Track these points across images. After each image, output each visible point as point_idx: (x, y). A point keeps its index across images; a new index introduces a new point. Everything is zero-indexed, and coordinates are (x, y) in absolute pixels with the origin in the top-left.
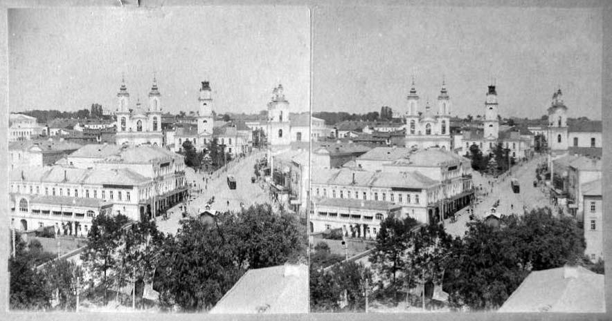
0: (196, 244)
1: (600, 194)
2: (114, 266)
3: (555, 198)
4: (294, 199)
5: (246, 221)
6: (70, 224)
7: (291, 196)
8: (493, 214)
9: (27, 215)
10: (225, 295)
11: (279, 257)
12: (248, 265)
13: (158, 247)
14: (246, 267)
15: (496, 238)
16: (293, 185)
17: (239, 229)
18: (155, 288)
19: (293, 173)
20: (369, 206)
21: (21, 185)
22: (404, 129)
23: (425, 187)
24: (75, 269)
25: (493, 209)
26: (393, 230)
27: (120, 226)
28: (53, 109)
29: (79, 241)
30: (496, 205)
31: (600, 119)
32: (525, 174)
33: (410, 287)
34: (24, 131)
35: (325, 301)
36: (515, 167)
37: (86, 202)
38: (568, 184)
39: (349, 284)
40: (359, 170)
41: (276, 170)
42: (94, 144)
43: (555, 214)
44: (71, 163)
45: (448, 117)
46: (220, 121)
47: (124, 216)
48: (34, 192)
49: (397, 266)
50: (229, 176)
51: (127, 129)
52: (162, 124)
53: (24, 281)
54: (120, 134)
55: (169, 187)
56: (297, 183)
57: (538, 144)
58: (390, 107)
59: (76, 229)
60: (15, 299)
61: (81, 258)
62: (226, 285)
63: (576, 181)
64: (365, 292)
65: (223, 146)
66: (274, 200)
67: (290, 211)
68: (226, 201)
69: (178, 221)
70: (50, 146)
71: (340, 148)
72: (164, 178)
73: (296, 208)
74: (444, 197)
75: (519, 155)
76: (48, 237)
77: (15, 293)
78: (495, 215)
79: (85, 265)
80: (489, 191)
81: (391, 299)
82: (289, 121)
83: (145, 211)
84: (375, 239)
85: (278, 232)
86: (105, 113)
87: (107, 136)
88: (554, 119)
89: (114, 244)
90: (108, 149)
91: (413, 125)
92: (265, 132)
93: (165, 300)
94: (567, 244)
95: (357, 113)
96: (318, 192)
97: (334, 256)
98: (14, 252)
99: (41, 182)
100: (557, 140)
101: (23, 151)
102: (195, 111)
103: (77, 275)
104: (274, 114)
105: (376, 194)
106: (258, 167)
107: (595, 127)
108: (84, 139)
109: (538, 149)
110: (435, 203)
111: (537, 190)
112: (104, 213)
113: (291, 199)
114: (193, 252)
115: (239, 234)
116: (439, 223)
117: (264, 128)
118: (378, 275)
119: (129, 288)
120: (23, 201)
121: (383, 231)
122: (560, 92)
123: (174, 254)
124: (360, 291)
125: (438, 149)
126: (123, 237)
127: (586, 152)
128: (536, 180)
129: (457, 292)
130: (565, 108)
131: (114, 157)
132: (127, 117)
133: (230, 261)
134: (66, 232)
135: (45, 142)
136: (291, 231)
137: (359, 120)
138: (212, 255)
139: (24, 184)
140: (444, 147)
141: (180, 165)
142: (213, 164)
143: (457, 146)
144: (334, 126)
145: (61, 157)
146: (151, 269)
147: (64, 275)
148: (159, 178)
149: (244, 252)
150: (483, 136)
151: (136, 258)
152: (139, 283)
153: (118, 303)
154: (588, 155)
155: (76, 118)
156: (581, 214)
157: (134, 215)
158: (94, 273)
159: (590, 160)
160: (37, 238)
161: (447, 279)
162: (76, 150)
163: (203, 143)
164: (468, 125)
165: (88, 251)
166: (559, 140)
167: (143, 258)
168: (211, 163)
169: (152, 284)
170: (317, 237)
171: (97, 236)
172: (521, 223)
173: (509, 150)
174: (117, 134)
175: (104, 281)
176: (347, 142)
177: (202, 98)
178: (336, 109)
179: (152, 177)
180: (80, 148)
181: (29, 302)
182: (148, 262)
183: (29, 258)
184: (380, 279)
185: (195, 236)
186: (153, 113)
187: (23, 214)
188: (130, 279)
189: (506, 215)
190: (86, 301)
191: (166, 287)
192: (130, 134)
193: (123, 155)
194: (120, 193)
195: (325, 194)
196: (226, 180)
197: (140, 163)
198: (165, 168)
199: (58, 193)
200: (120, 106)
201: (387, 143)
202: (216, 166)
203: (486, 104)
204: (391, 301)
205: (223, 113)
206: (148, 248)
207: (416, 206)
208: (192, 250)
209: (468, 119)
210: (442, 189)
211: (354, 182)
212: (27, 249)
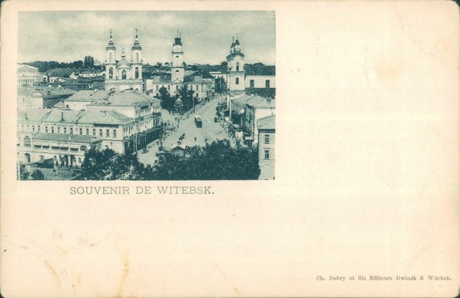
6: (66, 156)
8: (180, 146)
16: (247, 123)
22: (104, 75)
23: (122, 123)
25: (179, 142)
32: (206, 112)
36: (197, 106)
38: (245, 120)
43: (233, 145)
46: (189, 71)
51: (114, 78)
52: (143, 73)
54: (108, 81)
56: (250, 122)
58: (92, 56)
63: (252, 117)
72: (144, 118)
74: (138, 132)
75: (202, 95)
80: (175, 126)
88: (232, 64)
96: (34, 129)
100: (235, 82)
105: (81, 129)
117: (225, 76)
121: (87, 160)
125: (132, 91)
130: (242, 55)
135: (45, 89)
143: (148, 89)
144: (46, 73)
156: (256, 146)
160: (39, 168)
166: (237, 83)
172: (203, 154)
173: (193, 92)
176: (57, 86)
178: (48, 58)
187: (27, 149)
189: (190, 146)
193: (110, 98)
195: (39, 129)
196: (194, 120)
198: (144, 110)
201: (90, 87)
203: (173, 53)
211: (62, 119)
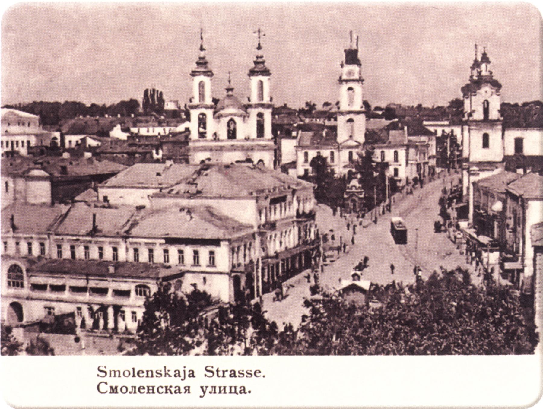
3: (475, 249)
6: (104, 308)
16: (508, 234)
22: (187, 130)
23: (228, 237)
28: (71, 99)
30: (361, 267)
32: (419, 213)
36: (397, 195)
38: (503, 227)
40: (104, 207)
45: (268, 106)
46: (377, 120)
47: (205, 293)
51: (209, 136)
59: (115, 315)
65: (385, 165)
71: (69, 168)
72: (278, 224)
74: (263, 254)
75: (405, 173)
78: (357, 283)
82: (502, 118)
83: (243, 283)
84: (135, 332)
88: (474, 106)
91: (202, 122)
102: (333, 103)
111: (442, 236)
116: (253, 302)
122: (485, 59)
128: (440, 219)
130: (496, 85)
137: (102, 115)
140: (261, 161)
143: (286, 159)
144: (57, 127)
145: (86, 188)
164: (307, 120)
170: (29, 331)
189: (380, 284)
201: (155, 156)
205: (383, 105)
210: (258, 239)
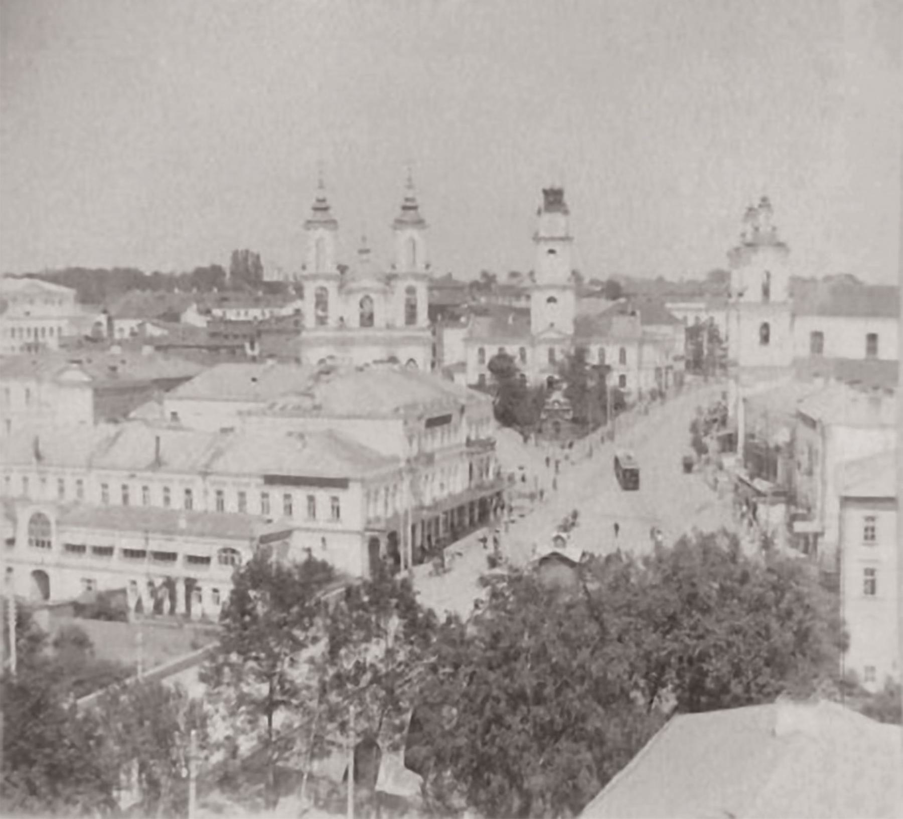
0: (526, 641)
1: (891, 493)
2: (295, 702)
3: (749, 504)
4: (804, 518)
5: (667, 580)
7: (793, 509)
8: (559, 550)
9: (48, 558)
10: (608, 786)
11: (761, 680)
12: (673, 702)
13: (417, 650)
14: (666, 707)
15: (569, 617)
16: (799, 478)
17: (649, 599)
18: (410, 765)
19: (801, 446)
20: (204, 524)
21: (33, 477)
22: (298, 312)
23: (359, 476)
24: (184, 709)
26: (268, 596)
27: (312, 592)
29: (196, 632)
31: (894, 282)
33: (313, 756)
34: (39, 324)
35: (81, 789)
36: (623, 417)
37: (216, 523)
39: (144, 743)
41: (752, 436)
42: (238, 361)
44: (174, 414)
48: (71, 494)
49: (278, 697)
50: (620, 453)
51: (332, 322)
53: (40, 736)
55: (450, 484)
56: (810, 473)
57: (698, 353)
59: (188, 598)
60: (15, 785)
61: (203, 678)
62: (610, 757)
64: (187, 766)
66: (746, 521)
67: (793, 553)
68: (611, 524)
69: (475, 578)
70: (114, 369)
71: (120, 370)
72: (437, 457)
73: (807, 544)
74: (414, 503)
76: (110, 618)
77: (15, 767)
79: (212, 698)
81: (262, 786)
82: (791, 301)
83: (383, 548)
85: (757, 610)
86: (270, 276)
87: (272, 340)
89: (294, 639)
90: (278, 377)
92: (722, 331)
93: (439, 797)
94: (789, 636)
95: (166, 269)
97: (105, 664)
98: (13, 661)
99: (90, 467)
101: (39, 380)
102: (525, 271)
103: (191, 724)
104: (747, 278)
106: (701, 428)
107: (874, 301)
108: (210, 348)
109: (696, 363)
110: (388, 521)
112: (266, 554)
113: (794, 518)
114: (518, 665)
115: (647, 614)
117: (719, 318)
118: (224, 718)
119: (337, 764)
120: (38, 519)
123: (464, 670)
124: (174, 763)
125: (396, 367)
126: (319, 621)
127: (853, 374)
128: (692, 453)
129: (449, 773)
131: (295, 400)
132: (332, 287)
133: (622, 690)
134: (158, 607)
135: (99, 357)
136: (795, 607)
137: (170, 290)
138: (572, 673)
139: (40, 472)
141: (481, 422)
142: (574, 420)
144: (101, 307)
145: (147, 399)
146: (400, 711)
147: (155, 723)
148: (423, 459)
149: (662, 667)
150: (528, 331)
151: (356, 680)
152: (366, 751)
153: (306, 803)
154: (857, 382)
155: (187, 290)
157: (351, 561)
158: (240, 721)
159: (863, 396)
161: (417, 735)
162: (188, 379)
163: (544, 359)
165: (221, 659)
167: (376, 679)
168: (569, 416)
169: (402, 753)
171: (247, 618)
174: (304, 334)
175: (266, 743)
177: (542, 234)
178: (98, 258)
179: (403, 456)
180: (197, 374)
181: (55, 793)
182: (390, 691)
183: (55, 677)
184: (230, 732)
185: (524, 621)
186: (405, 276)
187: (39, 557)
188: (340, 739)
190: (216, 796)
191: (440, 760)
192: (339, 334)
193: (321, 391)
194: (311, 499)
196: (611, 464)
197: (370, 416)
198: (438, 429)
199: (136, 499)
200: (311, 257)
202: (582, 425)
204: (259, 794)
205: (604, 278)
206: (390, 653)
207: (330, 526)
208: (516, 659)
209: (482, 281)
212: (49, 652)
